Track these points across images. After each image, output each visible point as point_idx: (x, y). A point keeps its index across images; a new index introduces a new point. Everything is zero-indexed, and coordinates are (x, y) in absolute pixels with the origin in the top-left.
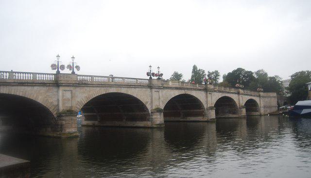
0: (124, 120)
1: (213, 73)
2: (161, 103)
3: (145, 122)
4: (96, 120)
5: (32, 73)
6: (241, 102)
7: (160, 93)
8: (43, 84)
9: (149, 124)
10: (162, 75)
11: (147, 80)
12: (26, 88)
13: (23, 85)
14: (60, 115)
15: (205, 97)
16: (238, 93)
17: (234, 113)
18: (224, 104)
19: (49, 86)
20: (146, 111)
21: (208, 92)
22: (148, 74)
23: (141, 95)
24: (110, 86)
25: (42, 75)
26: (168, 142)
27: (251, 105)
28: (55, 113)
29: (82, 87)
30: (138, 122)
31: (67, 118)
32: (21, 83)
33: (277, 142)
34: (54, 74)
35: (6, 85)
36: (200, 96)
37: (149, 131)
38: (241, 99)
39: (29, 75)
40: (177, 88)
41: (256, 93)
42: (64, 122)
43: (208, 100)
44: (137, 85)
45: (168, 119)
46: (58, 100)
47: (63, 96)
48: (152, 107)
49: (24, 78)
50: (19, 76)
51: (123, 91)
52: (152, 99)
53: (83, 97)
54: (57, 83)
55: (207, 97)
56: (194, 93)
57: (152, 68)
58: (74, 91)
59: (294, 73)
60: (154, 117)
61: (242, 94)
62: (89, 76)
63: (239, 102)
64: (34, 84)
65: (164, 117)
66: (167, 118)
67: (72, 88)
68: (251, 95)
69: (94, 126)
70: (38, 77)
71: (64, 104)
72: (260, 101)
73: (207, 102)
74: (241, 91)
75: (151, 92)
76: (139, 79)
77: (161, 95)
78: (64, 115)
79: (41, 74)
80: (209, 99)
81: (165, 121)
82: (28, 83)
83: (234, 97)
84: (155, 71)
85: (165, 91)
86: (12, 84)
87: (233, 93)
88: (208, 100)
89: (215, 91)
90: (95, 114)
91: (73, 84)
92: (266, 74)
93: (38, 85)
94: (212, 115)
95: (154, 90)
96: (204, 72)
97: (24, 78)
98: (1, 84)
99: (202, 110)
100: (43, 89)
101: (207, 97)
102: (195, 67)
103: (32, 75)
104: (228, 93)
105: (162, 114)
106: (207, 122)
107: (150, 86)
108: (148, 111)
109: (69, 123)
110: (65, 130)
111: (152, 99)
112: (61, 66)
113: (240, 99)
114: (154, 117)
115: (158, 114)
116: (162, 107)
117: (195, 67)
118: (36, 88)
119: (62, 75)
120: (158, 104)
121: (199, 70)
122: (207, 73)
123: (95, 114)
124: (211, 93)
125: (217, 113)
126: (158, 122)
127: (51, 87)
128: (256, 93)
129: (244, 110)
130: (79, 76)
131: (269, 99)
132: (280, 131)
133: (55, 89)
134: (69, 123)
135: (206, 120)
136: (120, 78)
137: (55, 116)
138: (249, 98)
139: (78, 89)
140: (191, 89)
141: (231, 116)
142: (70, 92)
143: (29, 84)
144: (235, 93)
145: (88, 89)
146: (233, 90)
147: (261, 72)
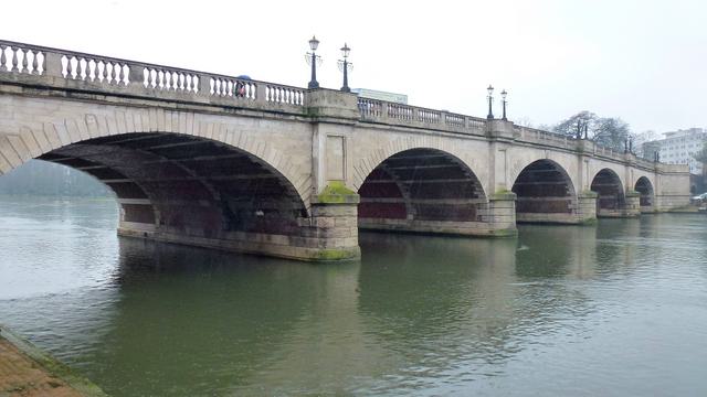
4: (151, 220)
5: (44, 50)
8: (279, 114)
9: (483, 228)
11: (480, 120)
12: (242, 121)
20: (477, 197)
21: (584, 158)
23: (468, 153)
24: (148, 101)
26: (360, 286)
29: (363, 130)
36: (565, 161)
37: (484, 245)
40: (535, 145)
42: (330, 222)
43: (496, 170)
45: (371, 222)
47: (327, 151)
50: (154, 79)
54: (311, 110)
55: (580, 168)
57: (507, 96)
59: (603, 109)
64: (261, 114)
66: (370, 220)
69: (146, 238)
75: (491, 151)
76: (270, 85)
79: (157, 68)
93: (269, 115)
95: (498, 146)
98: (6, 88)
99: (566, 199)
101: (580, 168)
103: (126, 69)
106: (580, 224)
110: (334, 243)
115: (505, 204)
119: (325, 93)
124: (587, 158)
131: (674, 178)
132: (87, 267)
133: (301, 129)
135: (576, 220)
139: (357, 133)
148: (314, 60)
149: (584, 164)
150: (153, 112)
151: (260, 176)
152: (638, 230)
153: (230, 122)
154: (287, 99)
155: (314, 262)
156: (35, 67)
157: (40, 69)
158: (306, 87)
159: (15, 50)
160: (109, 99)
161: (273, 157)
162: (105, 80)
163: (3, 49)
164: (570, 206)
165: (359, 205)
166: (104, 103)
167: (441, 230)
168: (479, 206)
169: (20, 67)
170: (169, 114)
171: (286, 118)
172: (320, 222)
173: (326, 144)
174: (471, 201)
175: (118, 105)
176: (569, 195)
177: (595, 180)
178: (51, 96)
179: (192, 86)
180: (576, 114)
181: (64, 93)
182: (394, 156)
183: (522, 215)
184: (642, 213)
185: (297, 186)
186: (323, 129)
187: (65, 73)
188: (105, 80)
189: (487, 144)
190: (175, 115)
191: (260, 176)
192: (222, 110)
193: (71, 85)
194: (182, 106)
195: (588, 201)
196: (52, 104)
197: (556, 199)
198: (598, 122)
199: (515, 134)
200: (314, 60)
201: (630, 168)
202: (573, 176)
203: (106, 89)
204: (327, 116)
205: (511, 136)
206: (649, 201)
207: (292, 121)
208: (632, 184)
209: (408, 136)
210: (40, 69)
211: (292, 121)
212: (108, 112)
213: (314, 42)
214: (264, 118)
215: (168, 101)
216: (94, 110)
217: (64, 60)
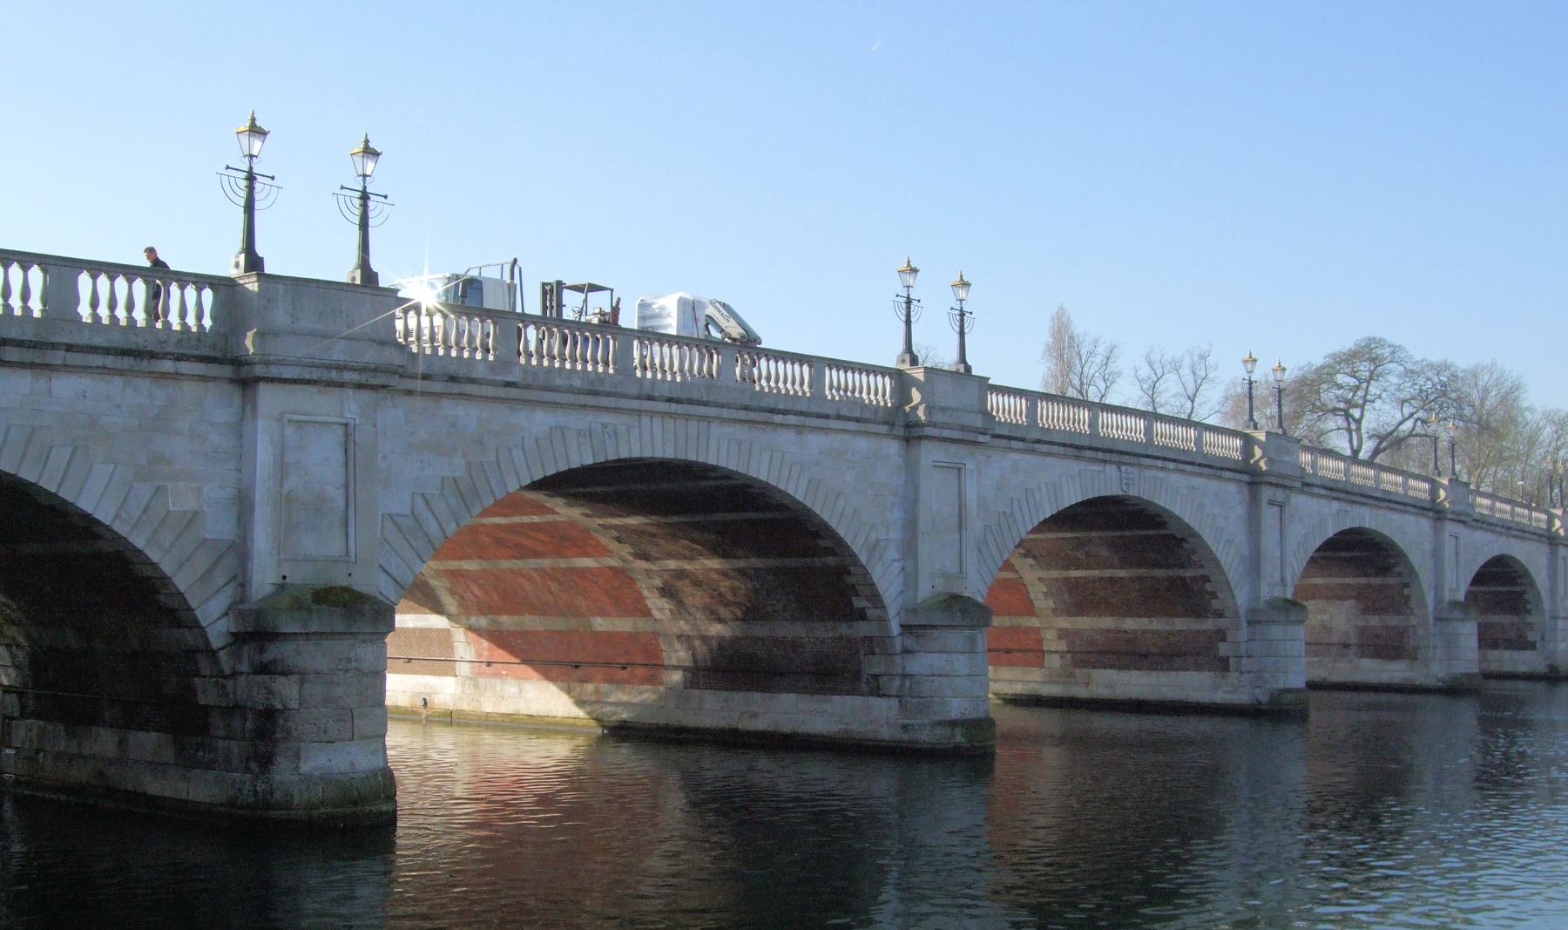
20: (862, 616)
38: (1449, 543)
39: (121, 283)
46: (243, 505)
55: (1254, 525)
67: (352, 405)
73: (1254, 564)
75: (240, 430)
77: (971, 495)
95: (929, 454)
98: (12, 354)
108: (883, 620)
118: (66, 386)
124: (1279, 495)
125: (1556, 625)
148: (365, 207)
149: (1269, 515)
151: (817, 562)
152: (1465, 761)
162: (113, 318)
163: (6, 267)
164: (1223, 649)
167: (761, 724)
168: (874, 644)
171: (145, 365)
173: (282, 449)
174: (844, 629)
176: (1219, 614)
177: (1479, 579)
179: (130, 307)
180: (1347, 343)
182: (1083, 503)
183: (1494, 654)
184: (1488, 676)
185: (182, 582)
186: (269, 398)
191: (817, 562)
198: (1410, 374)
200: (365, 207)
201: (1450, 528)
202: (1418, 558)
204: (282, 363)
206: (1531, 636)
207: (164, 376)
208: (1457, 584)
211: (164, 376)
214: (66, 368)
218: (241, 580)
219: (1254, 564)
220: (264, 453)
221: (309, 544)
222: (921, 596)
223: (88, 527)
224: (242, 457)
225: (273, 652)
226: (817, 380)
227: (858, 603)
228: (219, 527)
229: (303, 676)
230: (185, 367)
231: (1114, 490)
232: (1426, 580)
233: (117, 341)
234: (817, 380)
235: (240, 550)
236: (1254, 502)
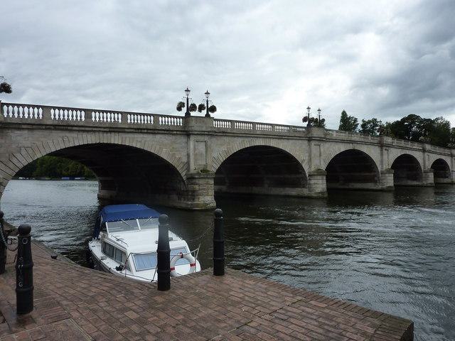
0: (266, 186)
1: (369, 122)
2: (322, 163)
3: (300, 189)
6: (192, 167)
7: (322, 147)
8: (168, 131)
9: (305, 192)
10: (213, 109)
12: (145, 136)
13: (67, 130)
14: (191, 178)
15: (379, 155)
16: (424, 151)
17: (415, 179)
18: (405, 166)
19: (177, 134)
21: (384, 148)
22: (305, 119)
25: (31, 109)
27: (440, 167)
28: (184, 173)
29: (219, 138)
30: (287, 189)
31: (201, 182)
32: (138, 129)
33: (325, 266)
34: (182, 117)
35: (119, 132)
36: (373, 152)
38: (427, 157)
39: (79, 112)
41: (446, 150)
42: (197, 187)
43: (314, 159)
44: (155, 129)
46: (188, 155)
48: (310, 167)
49: (26, 116)
51: (273, 143)
52: (310, 156)
53: (220, 152)
55: (382, 155)
56: (365, 149)
58: (209, 143)
60: (312, 182)
61: (429, 152)
62: (229, 121)
63: (424, 165)
65: (327, 182)
67: (206, 138)
68: (441, 154)
70: (95, 117)
71: (196, 160)
72: (452, 162)
73: (382, 162)
74: (428, 147)
75: (187, 143)
77: (322, 150)
78: (197, 177)
79: (165, 116)
80: (385, 157)
81: (328, 189)
82: (147, 129)
83: (418, 156)
84: (314, 115)
85: (327, 145)
86: (126, 130)
87: (416, 150)
88: (314, 159)
89: (393, 147)
90: (222, 176)
91: (208, 132)
92: (447, 124)
94: (389, 181)
95: (313, 143)
96: (356, 120)
97: (26, 116)
99: (373, 174)
100: (166, 139)
101: (382, 155)
102: (344, 114)
104: (410, 149)
105: (325, 178)
107: (185, 130)
108: (305, 174)
109: (204, 189)
111: (310, 156)
112: (200, 105)
113: (425, 158)
114: (312, 182)
115: (319, 177)
116: (324, 167)
117: (344, 114)
118: (158, 137)
120: (319, 164)
121: (350, 118)
122: (360, 122)
123: (222, 176)
125: (396, 178)
126: (319, 190)
127: (178, 137)
128: (447, 151)
129: (431, 176)
130: (215, 120)
133: (183, 139)
134: (204, 189)
136: (267, 124)
137: (184, 178)
138: (438, 157)
139: (214, 139)
140: (361, 143)
141: (410, 183)
142: (203, 144)
143: (149, 131)
144: (419, 150)
145: (226, 139)
146: (416, 146)
147: (439, 121)
150: (97, 134)
153: (139, 137)
154: (293, 128)
155: (301, 197)
156: (38, 115)
157: (41, 116)
158: (337, 128)
159: (8, 107)
160: (74, 128)
161: (164, 154)
165: (214, 178)
166: (71, 130)
169: (31, 116)
170: (105, 134)
172: (190, 187)
174: (298, 176)
175: (79, 131)
178: (46, 129)
181: (52, 127)
186: (192, 138)
187: (52, 117)
188: (19, 116)
189: (306, 142)
190: (109, 134)
192: (134, 131)
193: (56, 123)
194: (113, 130)
195: (387, 175)
196: (46, 133)
197: (367, 174)
199: (326, 135)
202: (420, 160)
203: (72, 124)
205: (323, 136)
208: (429, 164)
209: (250, 139)
210: (41, 116)
212: (74, 135)
213: (308, 108)
214: (158, 133)
215: (105, 128)
216: (67, 134)
217: (52, 111)
218: (188, 169)
219: (382, 162)
220: (192, 146)
221: (200, 162)
222: (312, 170)
223: (162, 160)
224: (188, 148)
225: (194, 181)
226: (156, 120)
227: (300, 171)
228: (185, 160)
229: (199, 185)
230: (178, 133)
231: (248, 145)
232: (378, 164)
233: (107, 125)
234: (156, 120)
235: (188, 163)
236: (382, 150)
